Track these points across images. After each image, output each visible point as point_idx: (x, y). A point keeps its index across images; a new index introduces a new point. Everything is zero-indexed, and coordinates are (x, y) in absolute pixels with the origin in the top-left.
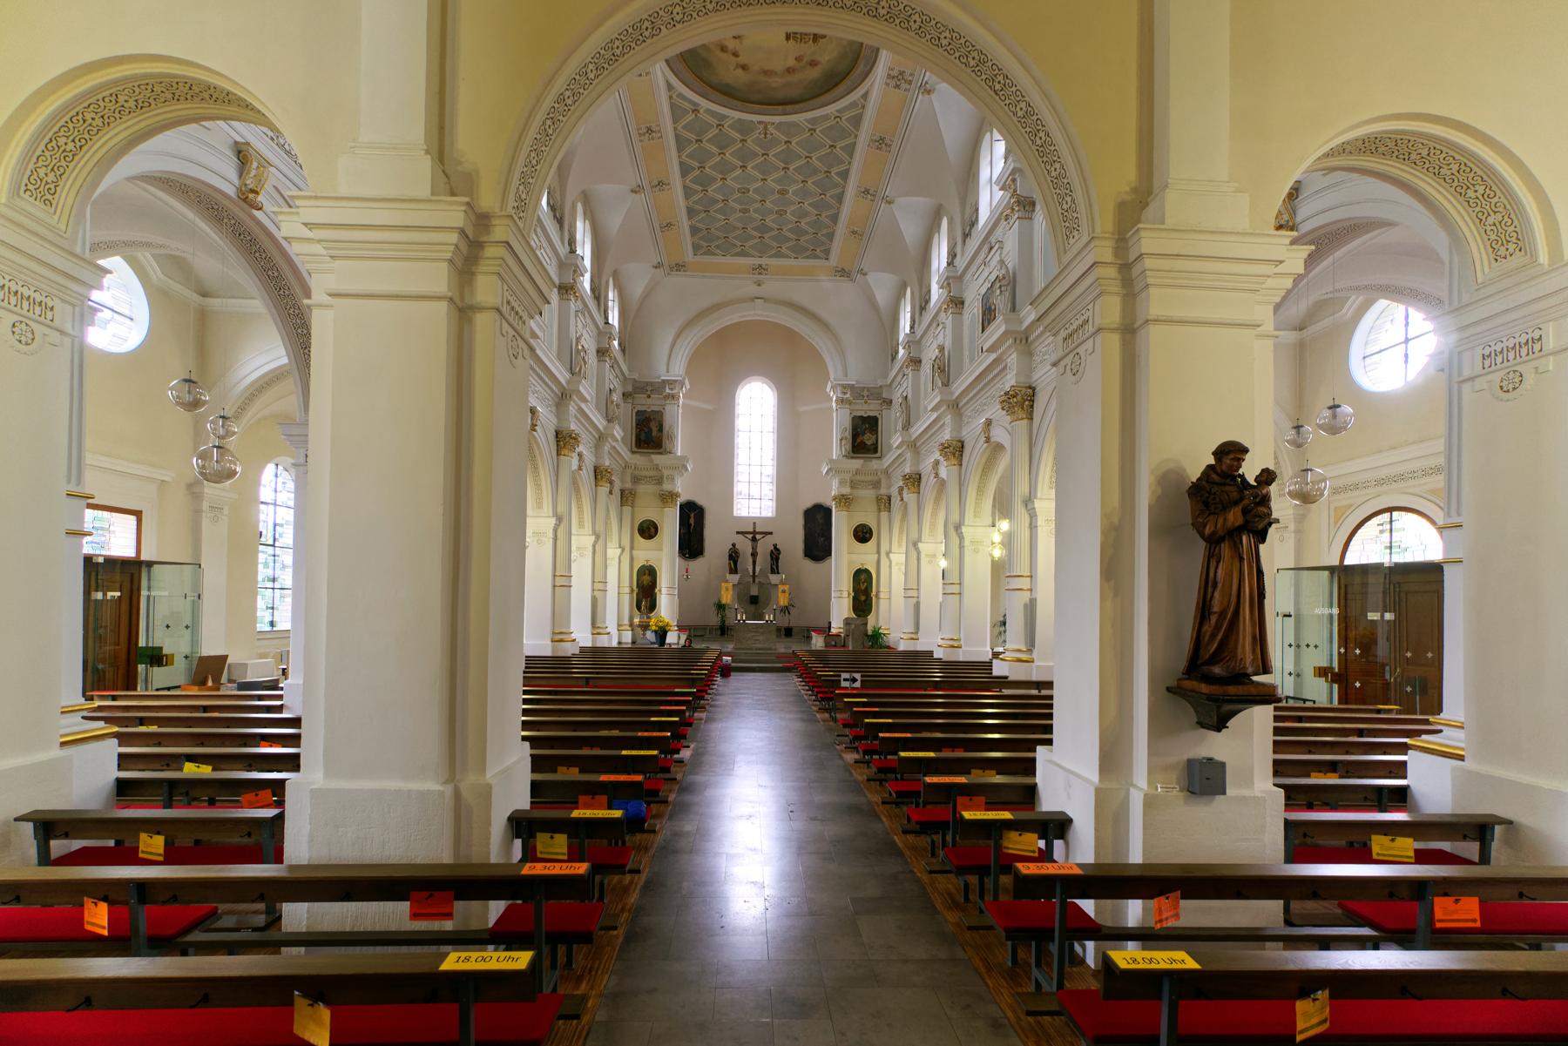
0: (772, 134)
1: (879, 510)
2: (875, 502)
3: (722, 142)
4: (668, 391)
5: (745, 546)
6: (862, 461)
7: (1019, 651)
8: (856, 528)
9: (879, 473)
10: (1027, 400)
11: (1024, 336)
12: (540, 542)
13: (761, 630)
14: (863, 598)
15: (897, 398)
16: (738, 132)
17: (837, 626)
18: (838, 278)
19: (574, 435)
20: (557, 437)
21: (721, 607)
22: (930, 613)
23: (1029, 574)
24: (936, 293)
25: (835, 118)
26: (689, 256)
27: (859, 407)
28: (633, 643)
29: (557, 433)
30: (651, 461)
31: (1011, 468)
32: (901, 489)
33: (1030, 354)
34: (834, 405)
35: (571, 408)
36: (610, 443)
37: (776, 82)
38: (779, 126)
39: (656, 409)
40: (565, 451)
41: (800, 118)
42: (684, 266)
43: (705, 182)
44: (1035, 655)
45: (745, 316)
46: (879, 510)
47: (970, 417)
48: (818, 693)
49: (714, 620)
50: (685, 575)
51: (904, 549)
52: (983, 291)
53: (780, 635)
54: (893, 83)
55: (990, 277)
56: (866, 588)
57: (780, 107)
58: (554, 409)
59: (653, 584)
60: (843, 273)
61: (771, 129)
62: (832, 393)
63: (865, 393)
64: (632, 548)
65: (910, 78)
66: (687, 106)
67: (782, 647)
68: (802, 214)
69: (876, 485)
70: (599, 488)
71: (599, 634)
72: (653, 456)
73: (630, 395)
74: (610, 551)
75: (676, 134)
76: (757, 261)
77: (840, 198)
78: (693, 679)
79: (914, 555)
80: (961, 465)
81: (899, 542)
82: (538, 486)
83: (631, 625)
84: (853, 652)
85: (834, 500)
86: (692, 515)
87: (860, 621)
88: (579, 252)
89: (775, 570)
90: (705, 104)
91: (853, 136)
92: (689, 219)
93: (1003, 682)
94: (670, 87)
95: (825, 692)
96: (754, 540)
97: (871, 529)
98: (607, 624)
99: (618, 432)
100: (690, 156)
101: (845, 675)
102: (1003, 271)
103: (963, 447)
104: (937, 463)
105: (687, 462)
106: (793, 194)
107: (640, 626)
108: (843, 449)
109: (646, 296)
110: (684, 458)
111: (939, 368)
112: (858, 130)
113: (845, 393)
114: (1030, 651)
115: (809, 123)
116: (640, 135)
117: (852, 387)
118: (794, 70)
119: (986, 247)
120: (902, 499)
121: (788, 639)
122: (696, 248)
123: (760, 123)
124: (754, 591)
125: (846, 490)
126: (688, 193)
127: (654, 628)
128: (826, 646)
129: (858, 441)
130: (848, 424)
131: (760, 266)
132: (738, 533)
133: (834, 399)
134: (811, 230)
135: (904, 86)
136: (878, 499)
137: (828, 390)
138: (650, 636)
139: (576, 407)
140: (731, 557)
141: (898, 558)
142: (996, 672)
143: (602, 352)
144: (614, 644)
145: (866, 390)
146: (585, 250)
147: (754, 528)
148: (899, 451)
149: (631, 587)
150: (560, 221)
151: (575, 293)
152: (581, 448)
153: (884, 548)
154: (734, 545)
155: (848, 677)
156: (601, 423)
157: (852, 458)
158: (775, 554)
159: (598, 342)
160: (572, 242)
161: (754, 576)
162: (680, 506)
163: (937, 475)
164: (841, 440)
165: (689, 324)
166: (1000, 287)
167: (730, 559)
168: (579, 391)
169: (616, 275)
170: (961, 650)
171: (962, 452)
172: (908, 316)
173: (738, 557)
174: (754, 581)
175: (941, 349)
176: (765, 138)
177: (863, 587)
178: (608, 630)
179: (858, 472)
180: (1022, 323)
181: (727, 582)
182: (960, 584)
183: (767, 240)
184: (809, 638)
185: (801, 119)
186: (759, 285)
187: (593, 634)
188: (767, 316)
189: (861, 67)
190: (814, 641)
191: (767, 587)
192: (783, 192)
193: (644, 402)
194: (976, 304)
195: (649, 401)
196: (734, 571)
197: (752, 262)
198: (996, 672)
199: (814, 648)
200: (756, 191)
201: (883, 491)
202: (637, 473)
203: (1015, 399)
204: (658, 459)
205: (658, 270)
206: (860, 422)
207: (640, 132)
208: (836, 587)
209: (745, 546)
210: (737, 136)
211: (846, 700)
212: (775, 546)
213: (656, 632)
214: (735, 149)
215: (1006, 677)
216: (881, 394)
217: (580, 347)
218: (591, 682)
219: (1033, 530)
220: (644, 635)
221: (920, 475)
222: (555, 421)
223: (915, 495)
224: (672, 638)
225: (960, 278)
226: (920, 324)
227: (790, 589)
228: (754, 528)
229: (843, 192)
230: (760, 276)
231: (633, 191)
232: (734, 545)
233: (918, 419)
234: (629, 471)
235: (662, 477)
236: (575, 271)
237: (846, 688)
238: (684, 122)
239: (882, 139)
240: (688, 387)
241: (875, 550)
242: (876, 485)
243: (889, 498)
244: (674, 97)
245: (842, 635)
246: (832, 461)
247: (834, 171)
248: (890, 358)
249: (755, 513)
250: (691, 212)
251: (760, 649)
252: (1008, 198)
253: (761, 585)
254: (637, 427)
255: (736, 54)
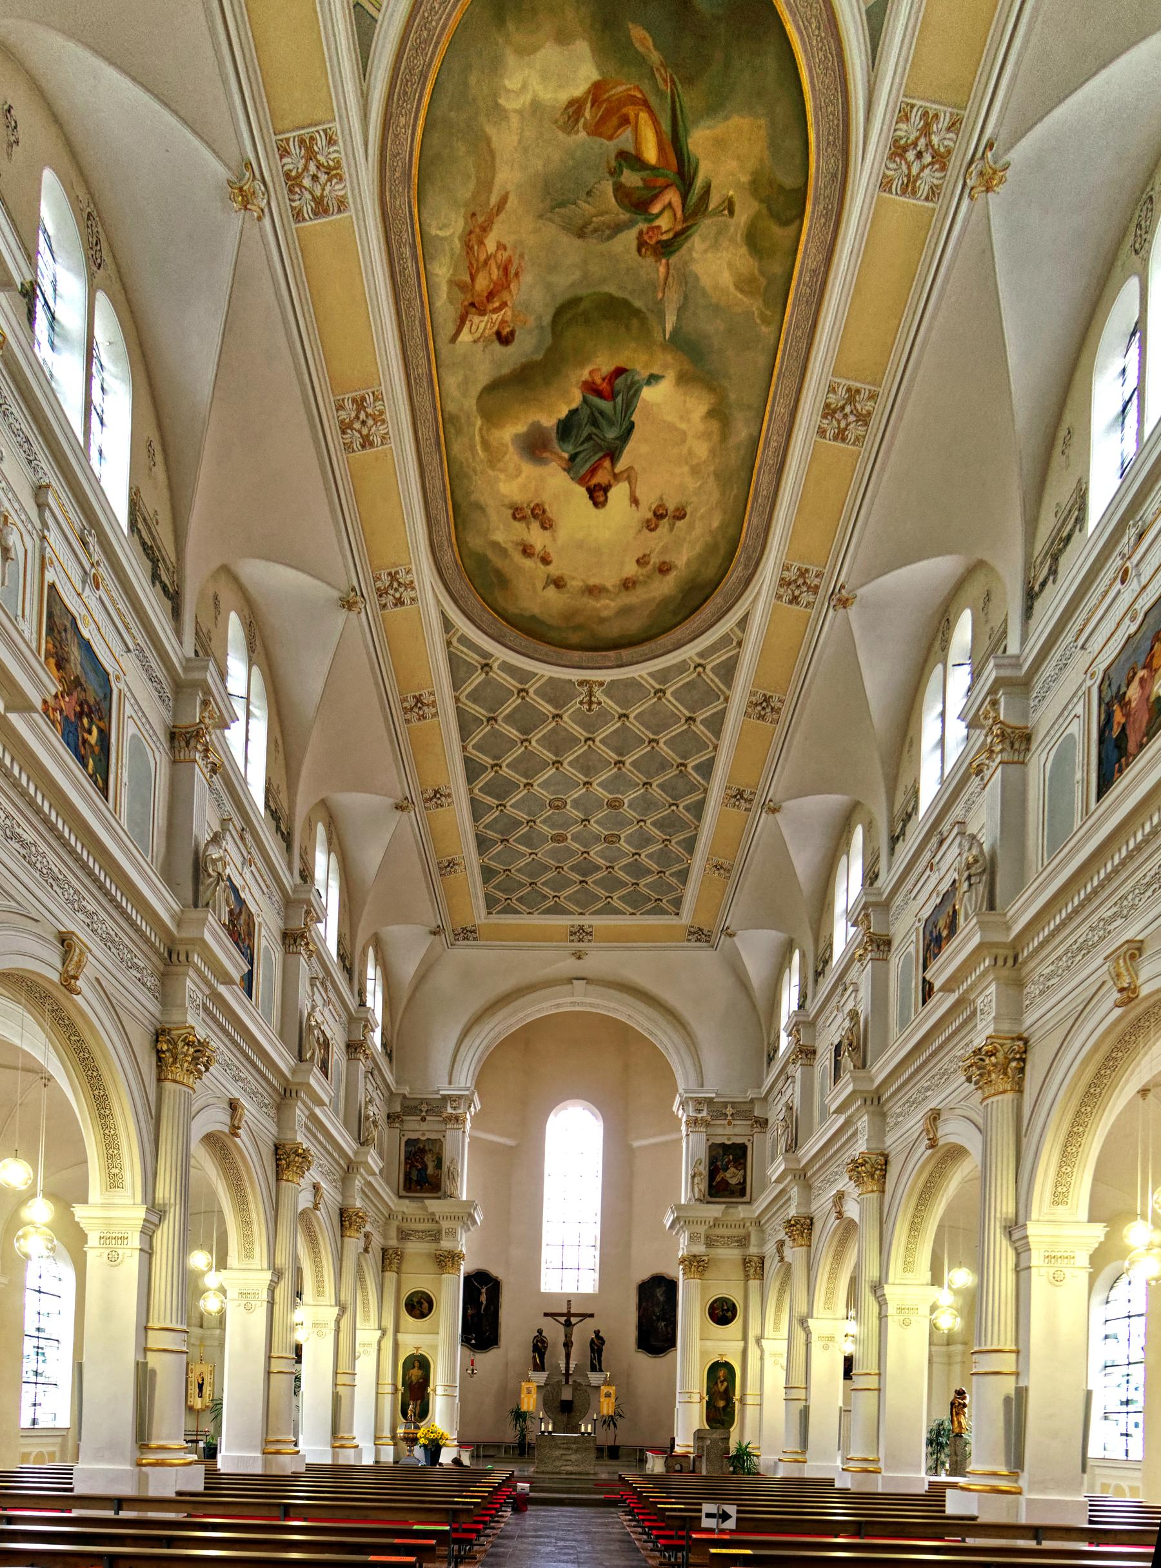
0: (599, 703)
1: (747, 1278)
2: (741, 1267)
3: (526, 721)
4: (450, 1110)
5: (554, 1332)
6: (723, 1206)
7: (994, 1474)
8: (715, 1301)
9: (748, 1224)
10: (1014, 1059)
11: (1011, 954)
12: (248, 1308)
13: (574, 1446)
14: (722, 1404)
15: (776, 1113)
16: (548, 702)
17: (684, 1443)
18: (693, 944)
19: (300, 1151)
20: (277, 1154)
21: (519, 1416)
22: (824, 1422)
23: (1014, 1348)
24: (842, 935)
25: (695, 668)
26: (479, 915)
27: (720, 1131)
28: (396, 1462)
29: (277, 1147)
30: (425, 1208)
31: (985, 1177)
32: (781, 1244)
33: (1019, 984)
34: (683, 1127)
35: (298, 1111)
36: (362, 1175)
37: (607, 606)
38: (611, 688)
39: (433, 1136)
40: (288, 1175)
41: (641, 672)
42: (474, 932)
43: (501, 789)
44: (1023, 1482)
45: (558, 1005)
46: (747, 1278)
47: (820, 1188)
48: (658, 1537)
49: (510, 1435)
50: (470, 1371)
51: (784, 1333)
52: (926, 913)
53: (602, 1457)
54: (787, 595)
55: (940, 888)
56: (726, 1390)
57: (611, 653)
58: (273, 1112)
59: (425, 1381)
60: (699, 935)
61: (599, 695)
62: (681, 1112)
63: (729, 1111)
64: (397, 1330)
65: (816, 581)
66: (474, 658)
67: (604, 1472)
68: (645, 840)
69: (743, 1242)
70: (283, 1183)
71: (342, 1447)
72: (427, 1202)
73: (398, 1117)
74: (361, 1336)
75: (458, 708)
76: (575, 921)
77: (698, 809)
78: (455, 1511)
79: (800, 1335)
80: (883, 1191)
81: (775, 1323)
82: (246, 1223)
83: (394, 1437)
84: (706, 1478)
85: (682, 1262)
86: (484, 1290)
87: (717, 1435)
88: (369, 1004)
89: (596, 1367)
90: (501, 654)
91: (722, 699)
92: (480, 854)
93: (968, 1525)
94: (447, 625)
95: (671, 1537)
96: (568, 1324)
97: (734, 1305)
98: (355, 1434)
99: (374, 1160)
100: (474, 697)
101: (708, 1508)
102: (974, 851)
103: (886, 1163)
104: (840, 1197)
105: (475, 1209)
106: (630, 806)
107: (405, 1439)
108: (696, 1190)
109: (422, 977)
110: (470, 1204)
111: (850, 1045)
112: (729, 687)
113: (699, 1111)
114: (1014, 1475)
115: (655, 680)
116: (406, 710)
117: (710, 1101)
118: (634, 583)
119: (934, 840)
120: (782, 1259)
121: (613, 1463)
122: (491, 903)
123: (582, 683)
124: (567, 1394)
125: (700, 1249)
126: (477, 810)
127: (422, 1441)
128: (667, 1472)
129: (718, 1179)
130: (703, 1154)
131: (581, 927)
132: (546, 1315)
133: (684, 1119)
134: (655, 867)
135: (806, 597)
136: (746, 1262)
137: (675, 1108)
138: (418, 1452)
139: (307, 1113)
140: (536, 1348)
141: (775, 1345)
142: (950, 1510)
143: (354, 1047)
144: (368, 1460)
145: (729, 1106)
146: (375, 1001)
147: (569, 1308)
148: (781, 1186)
149: (395, 1385)
150: (348, 971)
151: (307, 944)
152: (368, 1228)
153: (753, 1332)
154: (540, 1332)
155: (715, 1511)
156: (350, 1146)
157: (708, 1203)
158: (597, 1345)
159: (349, 1032)
160: (362, 993)
161: (567, 1375)
162: (468, 1279)
163: (840, 1215)
164: (693, 1177)
165: (477, 1020)
166: (969, 877)
167: (534, 1351)
168: (309, 1084)
169: (377, 942)
170: (879, 1476)
171: (886, 1170)
172: (795, 992)
173: (546, 1348)
174: (567, 1382)
175: (853, 1015)
176: (590, 710)
177: (722, 1388)
178: (356, 1442)
179: (716, 1223)
180: (1009, 928)
181: (529, 1381)
182: (879, 1374)
183: (591, 887)
184: (643, 1461)
185: (644, 673)
186: (579, 958)
187: (334, 1447)
188: (591, 1005)
189: (736, 572)
190: (649, 1465)
191: (586, 1392)
192: (614, 805)
193: (417, 1127)
194: (913, 938)
195: (424, 1126)
196: (539, 1367)
197: (570, 923)
198: (950, 1510)
199: (648, 1472)
200: (576, 804)
201: (753, 1250)
202: (405, 1226)
203: (993, 1059)
204: (434, 1205)
205: (437, 937)
206: (721, 1152)
207: (406, 704)
208: (682, 1387)
209: (554, 1332)
210: (548, 708)
211: (713, 1551)
212: (597, 1333)
213: (425, 1446)
214: (545, 731)
215: (974, 1518)
216: (752, 1111)
217: (314, 1023)
218: (292, 1512)
219: (1022, 1274)
220: (411, 1451)
221: (812, 1219)
222: (274, 1130)
223: (804, 1248)
224: (446, 1457)
225: (885, 906)
226: (814, 996)
227: (616, 1391)
228: (569, 1308)
229: (705, 798)
230: (581, 944)
231: (398, 807)
232: (540, 1332)
233: (810, 1134)
234: (395, 1224)
235: (439, 1232)
236: (308, 912)
237: (710, 1531)
238: (468, 688)
239: (767, 699)
240: (479, 1107)
241: (740, 1336)
242: (743, 1242)
243: (762, 1260)
244: (454, 641)
245: (692, 1456)
246: (679, 1207)
247: (692, 763)
248: (765, 1059)
249: (569, 1288)
250: (483, 844)
251: (571, 1473)
252: (982, 737)
253: (577, 1387)
254: (406, 1163)
255: (545, 561)
